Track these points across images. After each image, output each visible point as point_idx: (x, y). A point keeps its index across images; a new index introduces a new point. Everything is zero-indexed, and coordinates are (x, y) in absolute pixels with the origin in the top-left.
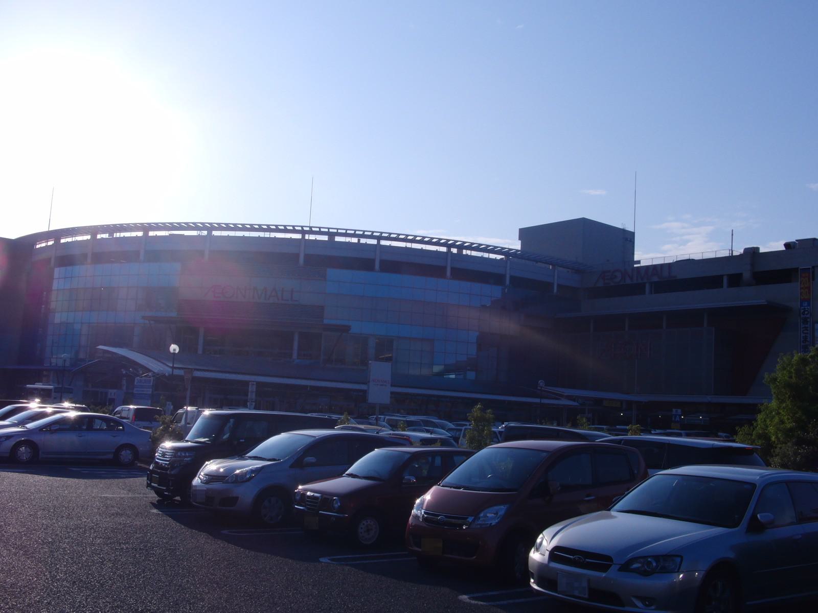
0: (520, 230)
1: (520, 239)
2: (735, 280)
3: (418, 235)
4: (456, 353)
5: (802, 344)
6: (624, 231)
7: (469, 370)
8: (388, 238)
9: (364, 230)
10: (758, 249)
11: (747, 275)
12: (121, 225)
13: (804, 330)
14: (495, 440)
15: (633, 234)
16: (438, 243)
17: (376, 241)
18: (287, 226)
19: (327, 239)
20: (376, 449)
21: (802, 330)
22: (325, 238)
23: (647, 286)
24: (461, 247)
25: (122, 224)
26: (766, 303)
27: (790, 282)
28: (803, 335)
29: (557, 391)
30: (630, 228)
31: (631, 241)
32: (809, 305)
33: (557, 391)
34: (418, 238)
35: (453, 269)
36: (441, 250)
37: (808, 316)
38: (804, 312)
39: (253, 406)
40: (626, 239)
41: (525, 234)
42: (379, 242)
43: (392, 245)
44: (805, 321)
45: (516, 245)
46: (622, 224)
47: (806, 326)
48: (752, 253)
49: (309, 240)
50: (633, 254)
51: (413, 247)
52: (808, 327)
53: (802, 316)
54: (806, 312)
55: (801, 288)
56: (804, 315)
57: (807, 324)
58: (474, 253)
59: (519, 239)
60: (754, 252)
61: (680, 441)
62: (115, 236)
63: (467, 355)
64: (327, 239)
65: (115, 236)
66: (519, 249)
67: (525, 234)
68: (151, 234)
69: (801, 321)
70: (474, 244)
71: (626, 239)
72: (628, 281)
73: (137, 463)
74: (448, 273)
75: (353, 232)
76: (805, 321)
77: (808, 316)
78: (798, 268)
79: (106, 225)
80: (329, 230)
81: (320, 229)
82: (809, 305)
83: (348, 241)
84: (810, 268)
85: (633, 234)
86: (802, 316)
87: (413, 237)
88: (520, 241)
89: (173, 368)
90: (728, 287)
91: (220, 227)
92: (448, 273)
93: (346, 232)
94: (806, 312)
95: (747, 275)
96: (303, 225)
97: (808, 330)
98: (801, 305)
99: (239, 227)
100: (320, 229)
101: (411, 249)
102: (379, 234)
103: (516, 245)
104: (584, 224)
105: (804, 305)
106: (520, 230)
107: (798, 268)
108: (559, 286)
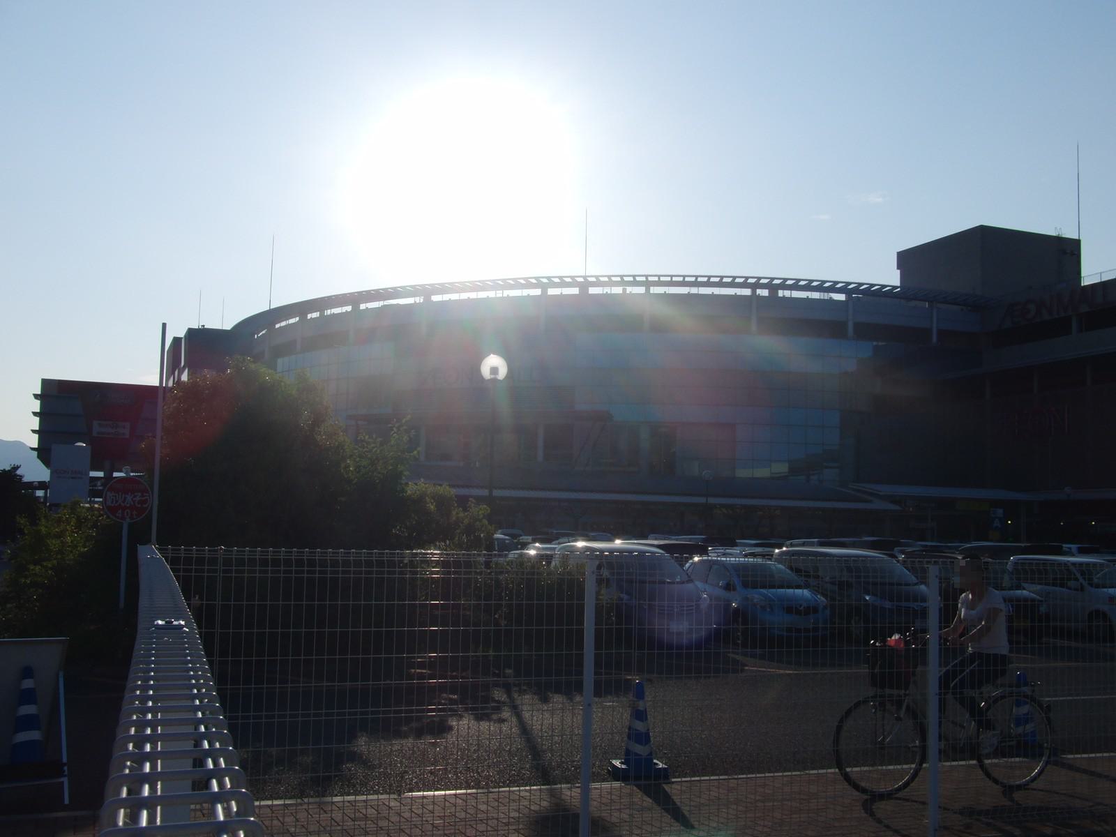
0: (898, 253)
1: (898, 268)
3: (852, 281)
6: (1059, 241)
8: (598, 284)
9: (709, 274)
12: (368, 292)
15: (1077, 243)
16: (833, 289)
17: (644, 288)
18: (589, 276)
19: (767, 295)
22: (575, 291)
25: (370, 291)
30: (1069, 233)
31: (1073, 254)
34: (789, 282)
41: (907, 259)
42: (754, 292)
43: (511, 295)
45: (890, 277)
46: (1056, 228)
51: (444, 299)
62: (318, 313)
64: (767, 295)
65: (318, 313)
66: (897, 282)
68: (781, 293)
70: (863, 284)
75: (693, 279)
79: (334, 296)
80: (659, 278)
81: (647, 278)
83: (526, 295)
84: (944, 755)
85: (1077, 243)
87: (781, 281)
88: (899, 271)
89: (800, 817)
93: (684, 279)
96: (698, 274)
99: (532, 283)
100: (647, 278)
102: (744, 279)
103: (890, 277)
104: (983, 233)
106: (898, 253)
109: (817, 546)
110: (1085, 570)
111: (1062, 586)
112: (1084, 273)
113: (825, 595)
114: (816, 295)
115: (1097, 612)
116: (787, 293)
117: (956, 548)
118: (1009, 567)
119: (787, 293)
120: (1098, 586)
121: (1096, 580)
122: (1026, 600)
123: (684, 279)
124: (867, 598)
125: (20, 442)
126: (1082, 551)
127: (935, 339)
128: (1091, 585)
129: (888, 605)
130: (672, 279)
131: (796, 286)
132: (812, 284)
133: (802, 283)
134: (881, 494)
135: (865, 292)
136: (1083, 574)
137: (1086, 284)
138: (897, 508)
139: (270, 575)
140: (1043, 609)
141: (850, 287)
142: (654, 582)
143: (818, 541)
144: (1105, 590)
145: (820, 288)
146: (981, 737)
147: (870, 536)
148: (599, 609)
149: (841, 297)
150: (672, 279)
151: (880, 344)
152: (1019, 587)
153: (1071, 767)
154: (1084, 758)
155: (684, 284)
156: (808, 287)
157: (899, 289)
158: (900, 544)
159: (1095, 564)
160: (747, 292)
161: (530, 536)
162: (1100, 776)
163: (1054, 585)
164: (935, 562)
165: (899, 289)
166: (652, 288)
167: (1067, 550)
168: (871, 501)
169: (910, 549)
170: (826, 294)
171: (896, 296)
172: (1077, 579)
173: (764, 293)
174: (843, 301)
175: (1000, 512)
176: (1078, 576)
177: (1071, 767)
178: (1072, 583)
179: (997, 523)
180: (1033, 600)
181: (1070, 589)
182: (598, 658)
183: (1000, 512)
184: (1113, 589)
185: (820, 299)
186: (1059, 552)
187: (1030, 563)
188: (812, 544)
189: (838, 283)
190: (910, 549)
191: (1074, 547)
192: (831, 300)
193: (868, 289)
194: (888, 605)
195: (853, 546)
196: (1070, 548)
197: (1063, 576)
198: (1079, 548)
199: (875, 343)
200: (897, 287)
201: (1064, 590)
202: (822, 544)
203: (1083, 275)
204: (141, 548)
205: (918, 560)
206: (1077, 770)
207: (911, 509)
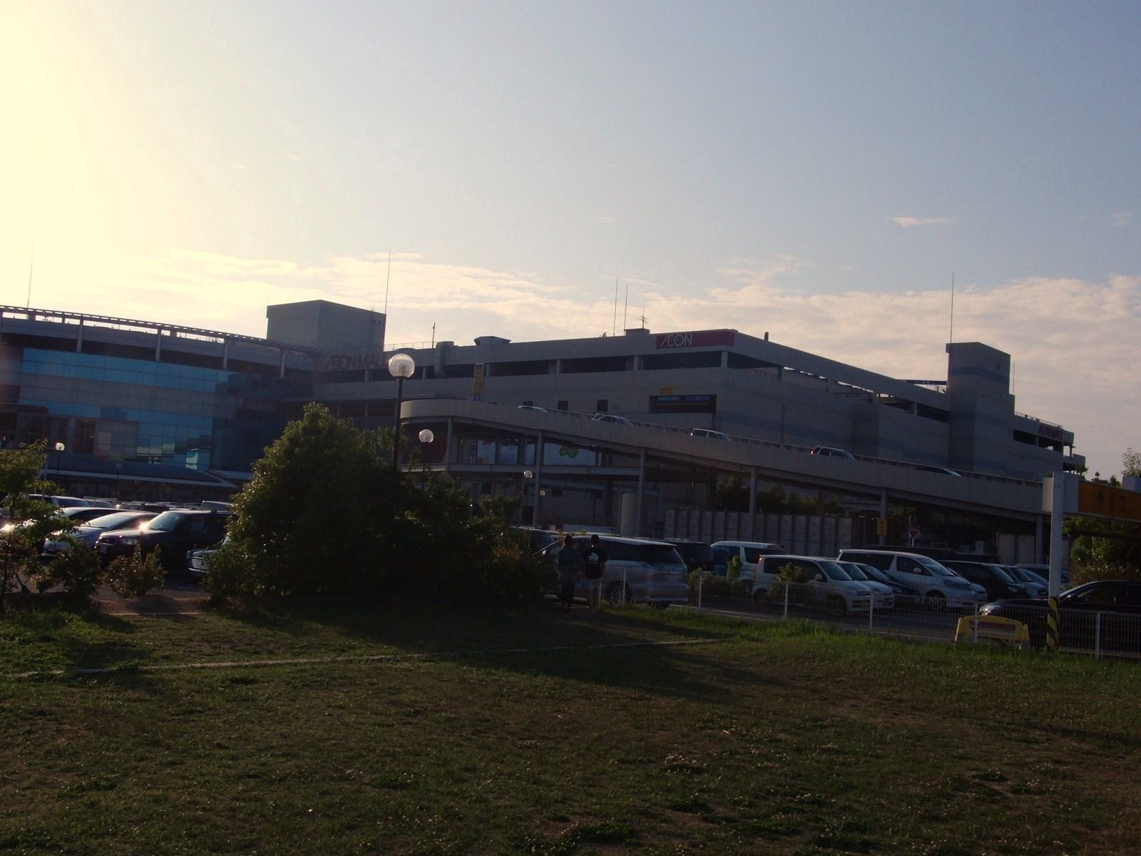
8: (91, 319)
10: (453, 343)
14: (136, 483)
15: (384, 316)
16: (216, 334)
17: (79, 321)
20: (1026, 626)
22: (24, 317)
23: (367, 372)
24: (173, 329)
30: (379, 308)
31: (380, 323)
35: (162, 352)
36: (202, 339)
39: (524, 532)
41: (277, 314)
42: (82, 322)
43: (132, 330)
45: (259, 330)
49: (69, 325)
50: (248, 340)
60: (446, 347)
61: (632, 542)
68: (179, 335)
72: (352, 368)
74: (158, 357)
78: (474, 365)
85: (384, 316)
91: (91, 319)
92: (158, 357)
95: (437, 368)
101: (186, 339)
107: (474, 365)
114: (203, 338)
116: (183, 335)
119: (183, 335)
123: (82, 322)
125: (978, 343)
127: (282, 373)
130: (63, 321)
146: (380, 814)
148: (990, 567)
150: (63, 321)
160: (155, 331)
166: (85, 321)
168: (220, 482)
173: (167, 333)
174: (256, 341)
182: (1095, 624)
185: (206, 341)
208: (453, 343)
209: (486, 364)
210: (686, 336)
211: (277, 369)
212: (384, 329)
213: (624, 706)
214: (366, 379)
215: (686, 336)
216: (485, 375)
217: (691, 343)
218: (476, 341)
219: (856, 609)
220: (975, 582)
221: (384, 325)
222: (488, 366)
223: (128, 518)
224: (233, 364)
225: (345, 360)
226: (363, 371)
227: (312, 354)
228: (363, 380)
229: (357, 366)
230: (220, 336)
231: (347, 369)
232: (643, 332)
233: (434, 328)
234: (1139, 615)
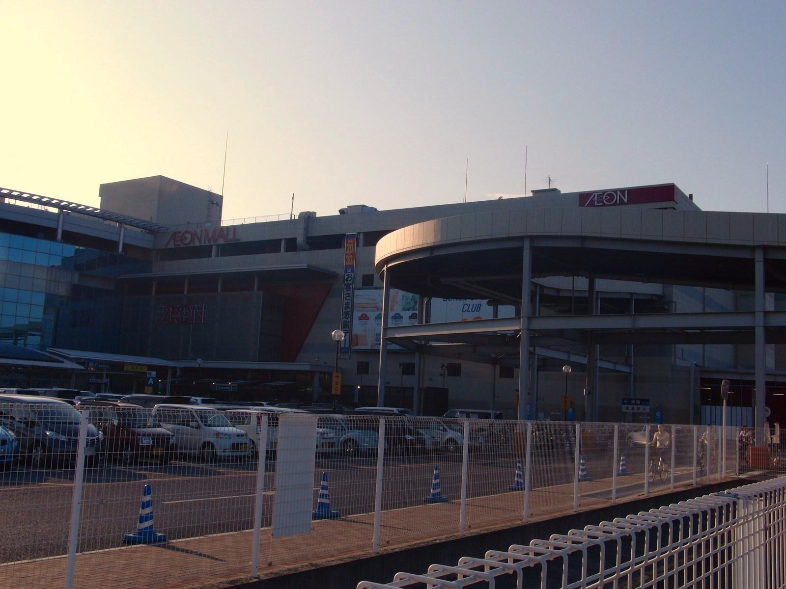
0: (100, 185)
2: (292, 245)
4: (16, 316)
5: (344, 310)
6: (210, 194)
7: (572, 354)
11: (300, 240)
12: (712, 327)
13: (347, 296)
16: (49, 203)
19: (57, 212)
21: (345, 296)
23: (214, 248)
26: (306, 267)
27: (341, 248)
28: (345, 301)
29: (61, 352)
30: (217, 191)
32: (352, 271)
33: (61, 352)
35: (64, 232)
37: (351, 282)
38: (348, 278)
40: (214, 202)
41: (107, 190)
44: (348, 287)
45: (94, 202)
47: (349, 293)
48: (308, 218)
52: (350, 294)
53: (346, 282)
54: (350, 279)
55: (347, 254)
56: (347, 281)
57: (350, 290)
58: (19, 203)
59: (99, 196)
63: (29, 318)
66: (98, 207)
67: (107, 190)
69: (345, 287)
71: (214, 202)
72: (197, 244)
73: (585, 388)
74: (59, 236)
76: (348, 287)
77: (351, 282)
82: (352, 271)
84: (355, 235)
86: (346, 282)
87: (19, 193)
88: (100, 198)
90: (285, 252)
92: (59, 236)
94: (350, 279)
95: (300, 240)
97: (350, 297)
98: (346, 271)
105: (348, 271)
106: (101, 185)
108: (125, 245)
109: (16, 394)
110: (203, 415)
111: (188, 425)
112: (223, 218)
113: (13, 430)
114: (35, 206)
115: (209, 442)
116: (12, 202)
117: (119, 398)
118: (153, 412)
120: (210, 426)
121: (209, 422)
122: (164, 435)
124: (48, 434)
126: (204, 402)
128: (206, 425)
129: (63, 438)
131: (19, 197)
132: (42, 200)
133: (35, 198)
134: (71, 357)
135: (72, 209)
136: (201, 418)
137: (223, 226)
138: (82, 367)
139: (43, 420)
140: (172, 441)
141: (71, 206)
142: (66, 423)
143: (17, 390)
144: (214, 428)
145: (39, 201)
147: (59, 387)
149: (55, 210)
151: (81, 248)
152: (160, 426)
153: (173, 548)
154: (183, 541)
155: (39, 201)
156: (29, 199)
157: (99, 211)
158: (79, 394)
159: (209, 411)
161: (200, 396)
162: (192, 552)
163: (183, 425)
164: (86, 408)
165: (99, 211)
167: (195, 401)
168: (62, 362)
169: (84, 398)
170: (43, 206)
171: (96, 215)
172: (197, 421)
175: (154, 373)
176: (199, 419)
177: (173, 548)
178: (194, 424)
179: (151, 381)
180: (168, 435)
181: (193, 427)
183: (154, 373)
184: (219, 428)
186: (187, 402)
187: (182, 411)
188: (12, 392)
189: (53, 199)
190: (84, 398)
191: (199, 399)
192: (46, 212)
193: (92, 211)
194: (63, 438)
195: (45, 394)
196: (197, 400)
197: (187, 420)
198: (202, 400)
199: (77, 247)
200: (97, 209)
201: (189, 428)
202: (19, 393)
203: (222, 219)
204: (477, 415)
205: (98, 406)
206: (178, 550)
207: (92, 369)
208: (315, 213)
209: (358, 234)
210: (619, 193)
211: (115, 244)
212: (221, 211)
213: (282, 487)
214: (214, 254)
215: (619, 193)
216: (358, 246)
217: (626, 201)
218: (348, 207)
219: (150, 408)
220: (255, 406)
221: (221, 207)
222: (361, 236)
223: (592, 509)
224: (70, 237)
225: (189, 236)
226: (211, 247)
227: (152, 230)
228: (210, 256)
229: (203, 240)
230: (54, 205)
231: (191, 245)
232: (553, 192)
233: (293, 199)
234: (784, 459)
